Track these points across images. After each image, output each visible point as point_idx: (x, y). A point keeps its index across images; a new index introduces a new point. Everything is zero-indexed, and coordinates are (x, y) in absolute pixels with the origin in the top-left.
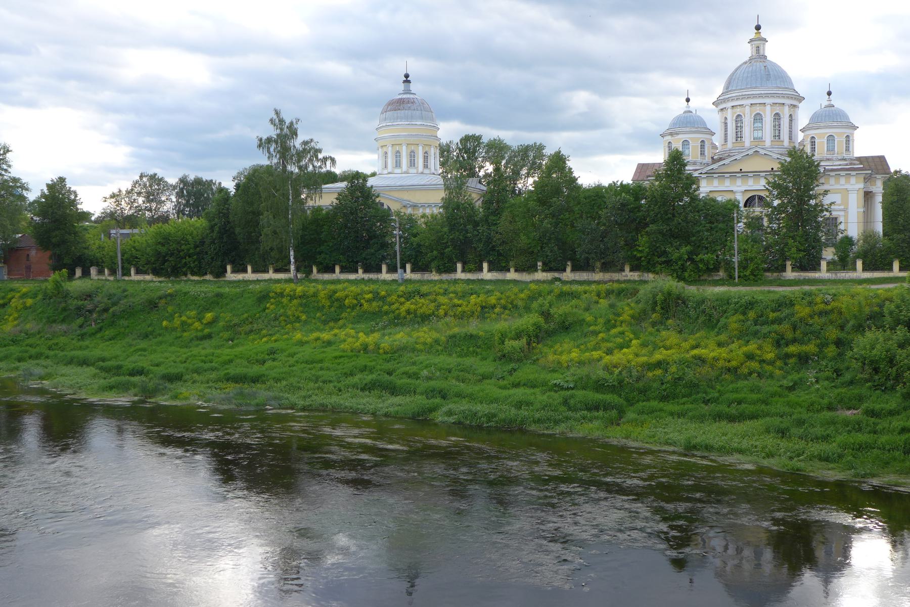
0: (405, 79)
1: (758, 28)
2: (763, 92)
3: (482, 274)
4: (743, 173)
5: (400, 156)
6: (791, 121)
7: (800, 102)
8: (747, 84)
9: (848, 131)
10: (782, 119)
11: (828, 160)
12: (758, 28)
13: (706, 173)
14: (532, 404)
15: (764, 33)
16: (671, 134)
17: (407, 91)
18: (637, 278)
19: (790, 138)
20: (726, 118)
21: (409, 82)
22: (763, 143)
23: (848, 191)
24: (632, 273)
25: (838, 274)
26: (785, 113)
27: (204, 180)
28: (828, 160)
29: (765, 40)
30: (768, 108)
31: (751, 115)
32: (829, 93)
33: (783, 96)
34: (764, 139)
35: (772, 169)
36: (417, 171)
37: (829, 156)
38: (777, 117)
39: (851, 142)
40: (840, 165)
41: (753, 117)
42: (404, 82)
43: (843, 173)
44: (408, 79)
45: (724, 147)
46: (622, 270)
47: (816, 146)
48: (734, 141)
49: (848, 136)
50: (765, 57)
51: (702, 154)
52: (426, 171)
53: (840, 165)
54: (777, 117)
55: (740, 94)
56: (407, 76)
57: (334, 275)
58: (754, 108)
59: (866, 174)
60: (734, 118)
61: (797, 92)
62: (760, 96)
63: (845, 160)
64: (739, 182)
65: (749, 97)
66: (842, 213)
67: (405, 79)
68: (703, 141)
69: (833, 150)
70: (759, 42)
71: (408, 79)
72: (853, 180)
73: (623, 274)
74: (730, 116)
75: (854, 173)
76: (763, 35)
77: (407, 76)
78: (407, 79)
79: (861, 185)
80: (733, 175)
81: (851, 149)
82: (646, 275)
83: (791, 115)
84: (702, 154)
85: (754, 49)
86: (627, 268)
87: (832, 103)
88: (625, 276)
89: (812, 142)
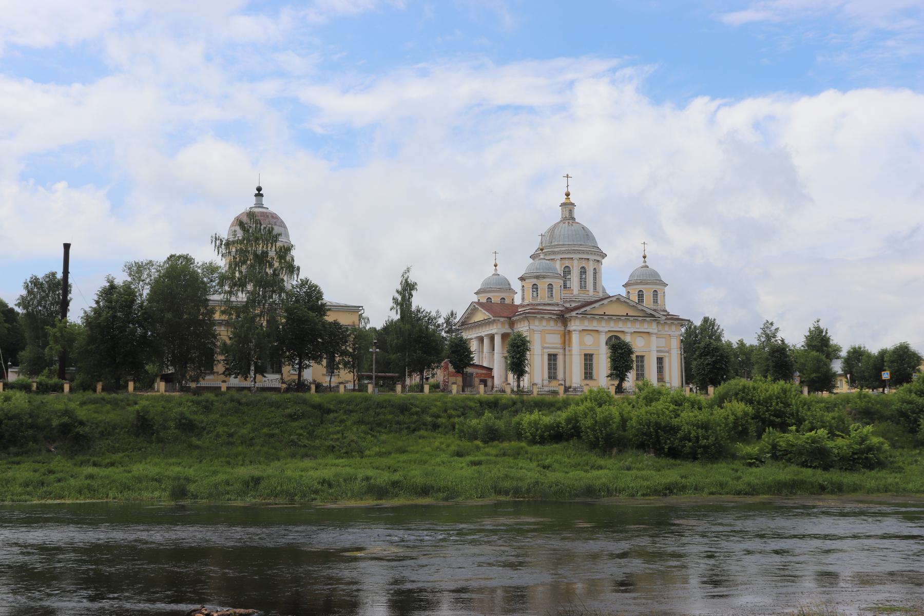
0: (257, 192)
1: (568, 194)
6: (595, 273)
7: (603, 258)
12: (568, 194)
13: (580, 314)
14: (643, 495)
16: (537, 277)
17: (259, 205)
19: (595, 288)
21: (262, 195)
26: (590, 268)
27: (24, 292)
29: (573, 204)
32: (645, 257)
34: (572, 288)
38: (583, 271)
42: (256, 195)
54: (583, 271)
56: (259, 189)
62: (569, 252)
64: (603, 323)
65: (579, 252)
66: (667, 354)
67: (257, 192)
76: (572, 200)
77: (259, 189)
78: (259, 194)
83: (595, 269)
87: (647, 264)
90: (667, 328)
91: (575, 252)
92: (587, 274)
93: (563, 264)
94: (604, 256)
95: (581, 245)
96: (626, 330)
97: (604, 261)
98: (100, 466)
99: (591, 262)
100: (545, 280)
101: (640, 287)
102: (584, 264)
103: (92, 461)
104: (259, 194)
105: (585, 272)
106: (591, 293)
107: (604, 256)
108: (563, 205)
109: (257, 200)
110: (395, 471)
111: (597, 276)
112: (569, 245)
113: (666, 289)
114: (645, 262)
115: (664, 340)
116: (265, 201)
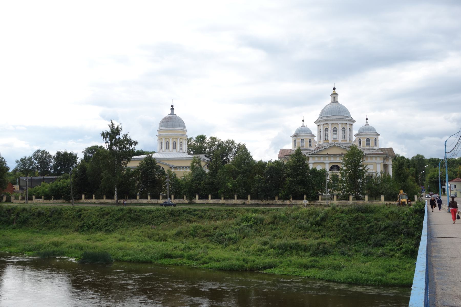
0: (171, 108)
1: (334, 89)
2: (337, 118)
3: (208, 200)
4: (328, 154)
5: (168, 143)
8: (330, 114)
9: (376, 137)
10: (346, 130)
11: (367, 149)
12: (334, 89)
13: (312, 154)
15: (337, 91)
17: (172, 113)
18: (281, 203)
19: (350, 139)
20: (320, 129)
21: (173, 109)
22: (337, 141)
23: (376, 164)
24: (278, 201)
25: (285, 201)
28: (367, 149)
29: (337, 94)
30: (340, 125)
31: (332, 128)
32: (303, 121)
33: (346, 120)
35: (342, 153)
36: (177, 151)
37: (368, 148)
39: (377, 142)
40: (372, 152)
41: (333, 129)
42: (171, 109)
43: (374, 156)
44: (173, 108)
45: (320, 142)
46: (275, 199)
47: (361, 143)
48: (324, 140)
49: (375, 139)
50: (338, 102)
51: (310, 145)
52: (181, 151)
53: (372, 152)
54: (344, 129)
55: (327, 119)
56: (172, 106)
57: (234, 201)
58: (333, 125)
59: (384, 156)
60: (324, 129)
61: (352, 118)
62: (336, 120)
63: (374, 149)
64: (327, 159)
65: (331, 120)
67: (171, 108)
68: (310, 140)
69: (369, 145)
70: (335, 95)
71: (173, 108)
72: (378, 159)
73: (275, 201)
74: (322, 128)
75: (379, 156)
77: (172, 106)
79: (382, 161)
80: (324, 156)
81: (377, 145)
82: (285, 202)
83: (350, 129)
84: (310, 145)
85: (333, 98)
86: (277, 198)
87: (304, 125)
88: (275, 202)
89: (359, 141)
90: (374, 159)
91: (339, 120)
92: (338, 131)
93: (325, 127)
94: (354, 121)
95: (333, 116)
96: (325, 162)
97: (354, 124)
98: (129, 242)
99: (348, 125)
100: (300, 137)
101: (368, 136)
102: (344, 126)
103: (2, 234)
104: (172, 109)
105: (328, 131)
106: (348, 141)
107: (354, 121)
108: (331, 95)
109: (171, 111)
110: (27, 236)
111: (351, 132)
112: (327, 116)
113: (379, 137)
114: (367, 122)
115: (373, 165)
116: (175, 112)
